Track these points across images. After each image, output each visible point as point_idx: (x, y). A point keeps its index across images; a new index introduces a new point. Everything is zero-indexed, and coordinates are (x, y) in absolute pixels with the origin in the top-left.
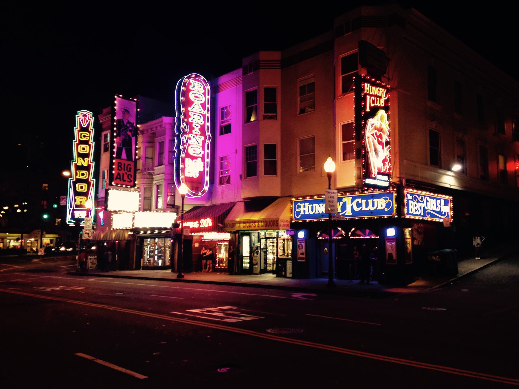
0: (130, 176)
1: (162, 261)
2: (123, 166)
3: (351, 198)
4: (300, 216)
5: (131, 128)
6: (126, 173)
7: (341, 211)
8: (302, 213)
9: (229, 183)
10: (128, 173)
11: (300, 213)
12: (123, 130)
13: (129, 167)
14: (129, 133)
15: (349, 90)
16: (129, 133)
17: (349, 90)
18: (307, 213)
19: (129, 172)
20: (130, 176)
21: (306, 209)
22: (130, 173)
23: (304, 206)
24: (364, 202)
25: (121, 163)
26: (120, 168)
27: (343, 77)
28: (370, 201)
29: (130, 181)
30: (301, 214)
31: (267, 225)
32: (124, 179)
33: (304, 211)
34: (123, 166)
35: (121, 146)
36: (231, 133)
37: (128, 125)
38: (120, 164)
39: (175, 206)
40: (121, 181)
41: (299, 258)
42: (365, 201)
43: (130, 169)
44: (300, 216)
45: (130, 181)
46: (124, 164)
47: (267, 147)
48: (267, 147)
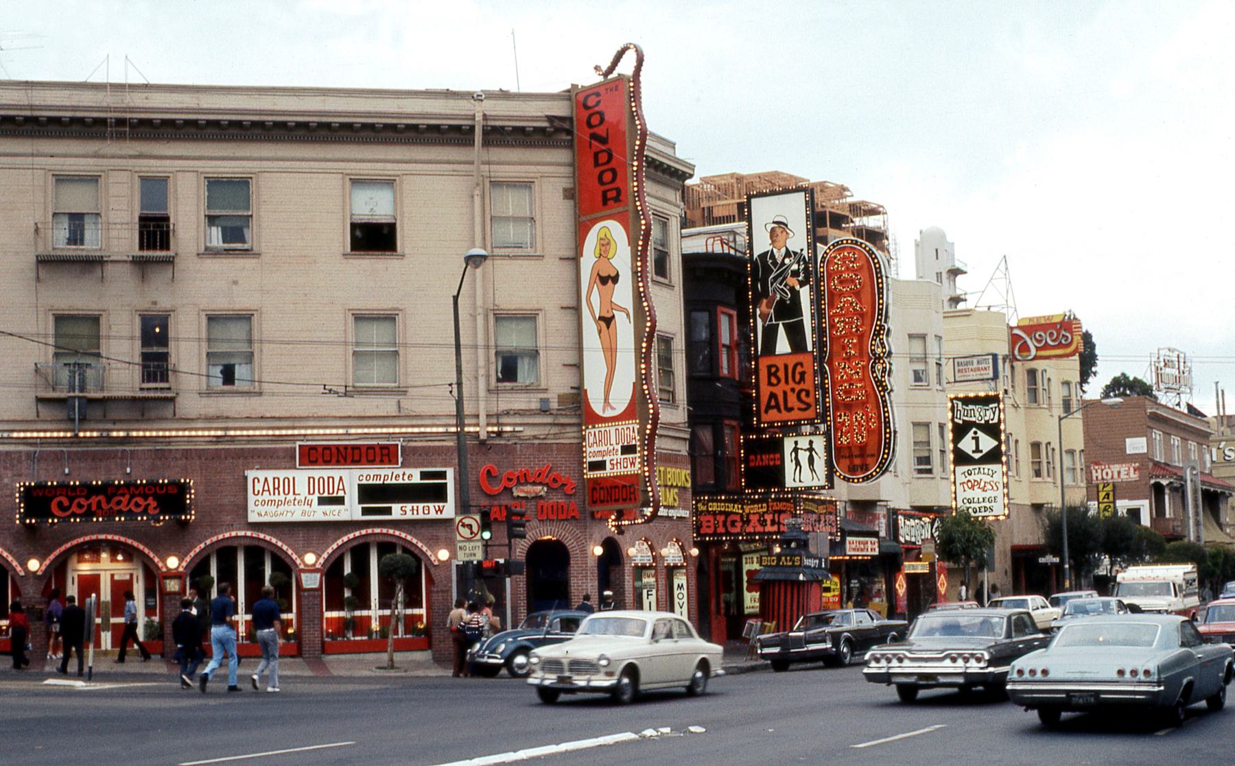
0: (803, 395)
2: (781, 374)
5: (795, 267)
6: (793, 390)
9: (392, 227)
10: (798, 388)
12: (775, 279)
13: (799, 369)
14: (792, 281)
15: (621, 158)
16: (792, 281)
17: (621, 158)
19: (799, 383)
20: (803, 395)
22: (802, 386)
25: (775, 366)
26: (774, 380)
29: (803, 406)
31: (340, 458)
32: (790, 405)
34: (781, 374)
35: (774, 322)
37: (787, 261)
38: (773, 370)
40: (779, 411)
43: (803, 374)
45: (803, 406)
46: (786, 367)
47: (363, 514)
48: (363, 514)
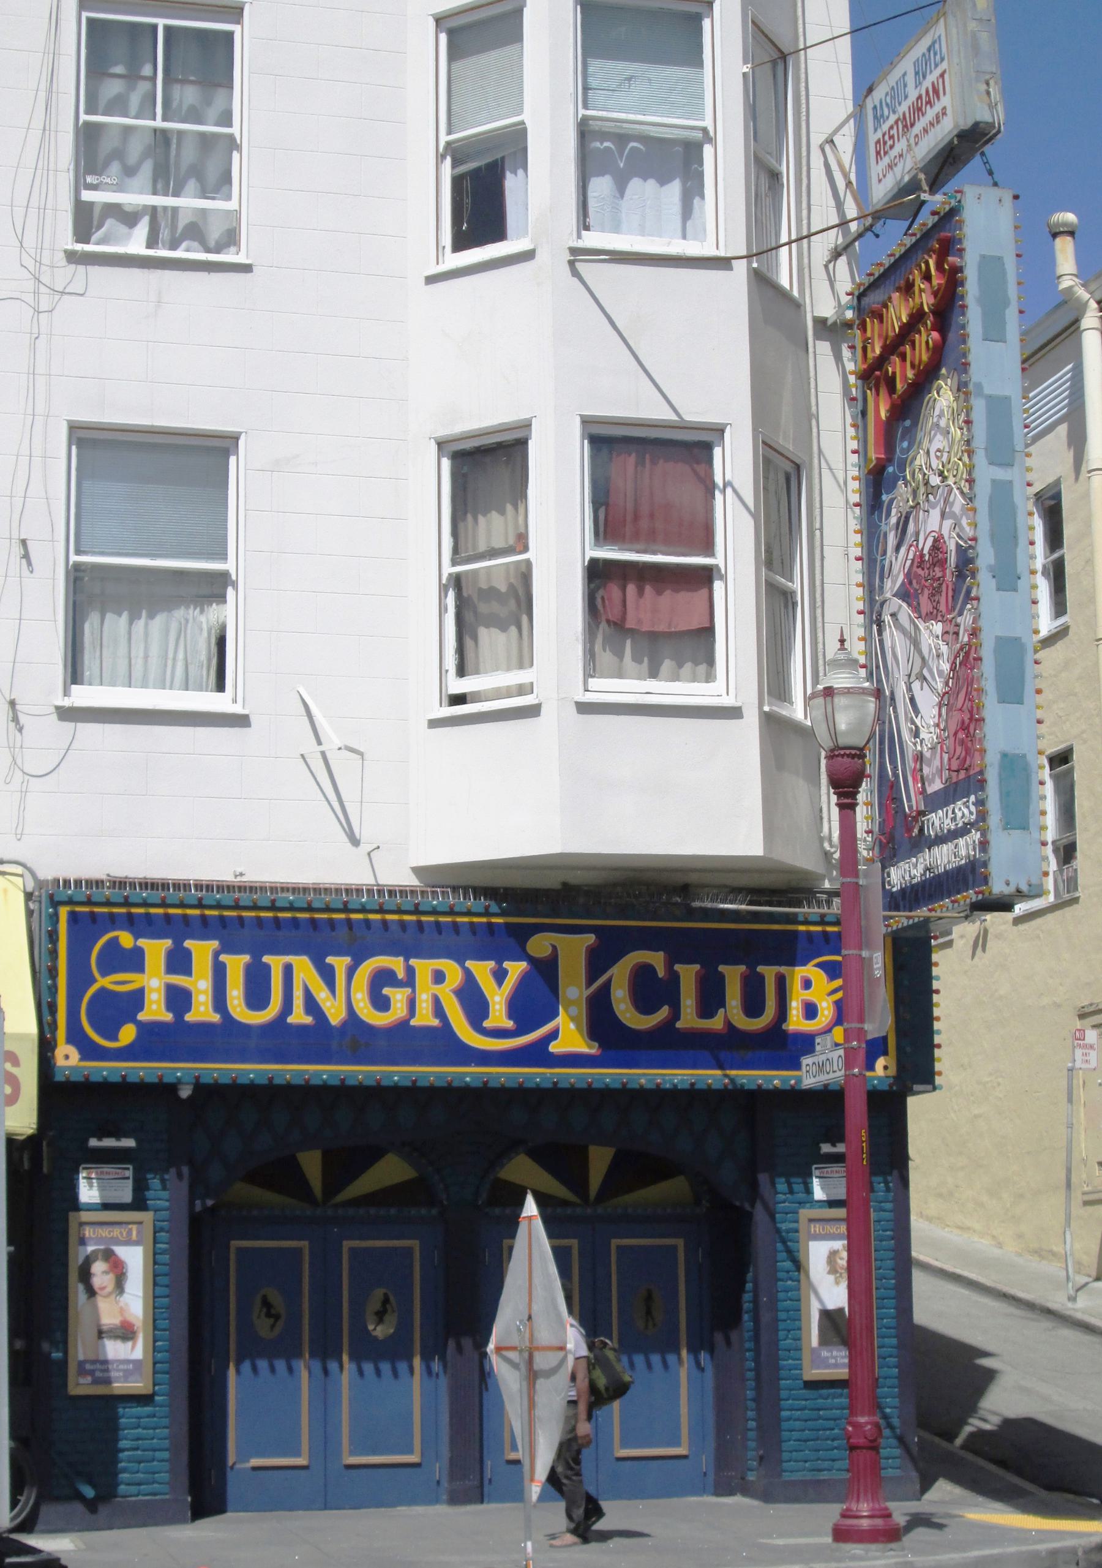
1: (72, 1551)
3: (590, 939)
4: (128, 1034)
7: (509, 1024)
8: (155, 1009)
11: (141, 1007)
18: (202, 1011)
21: (200, 985)
23: (179, 962)
24: (688, 974)
27: (520, 111)
28: (733, 975)
30: (141, 1017)
33: (178, 999)
36: (249, 275)
39: (425, 925)
41: (81, 1364)
42: (168, 943)
44: (128, 1034)
